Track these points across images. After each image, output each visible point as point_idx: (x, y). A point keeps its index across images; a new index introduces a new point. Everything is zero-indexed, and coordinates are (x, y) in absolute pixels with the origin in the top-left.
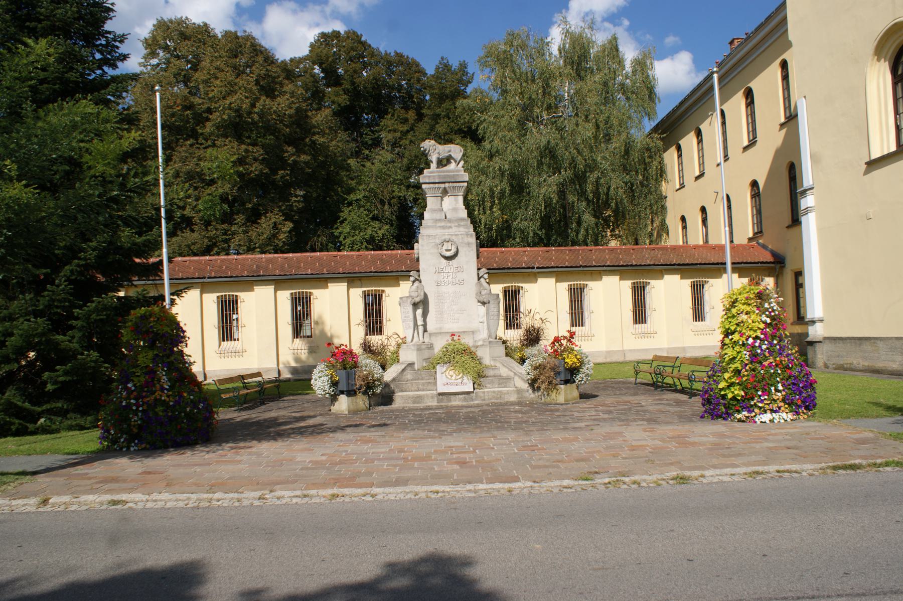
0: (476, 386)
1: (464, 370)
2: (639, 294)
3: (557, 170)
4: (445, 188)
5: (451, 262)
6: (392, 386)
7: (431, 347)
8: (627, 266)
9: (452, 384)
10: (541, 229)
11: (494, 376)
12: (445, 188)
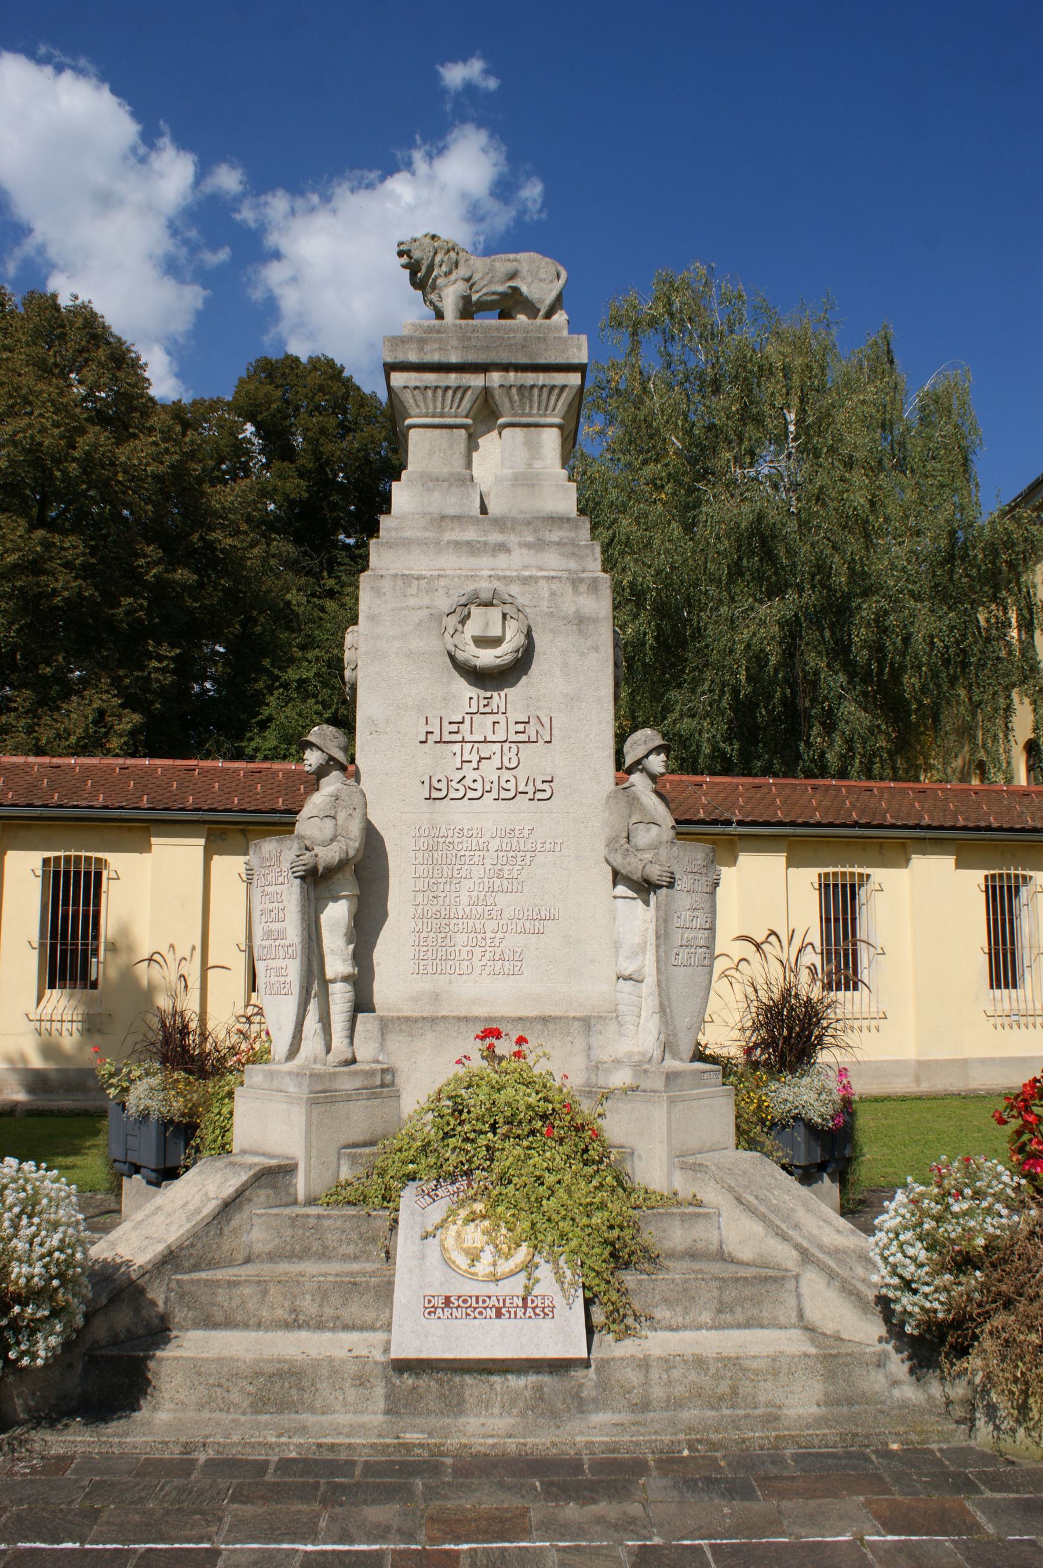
0: (599, 1316)
1: (536, 1223)
2: (1002, 903)
3: (776, 590)
4: (486, 390)
5: (497, 699)
6: (157, 1294)
7: (384, 1083)
8: (977, 828)
9: (472, 1307)
10: (728, 740)
11: (692, 1255)
12: (486, 390)
